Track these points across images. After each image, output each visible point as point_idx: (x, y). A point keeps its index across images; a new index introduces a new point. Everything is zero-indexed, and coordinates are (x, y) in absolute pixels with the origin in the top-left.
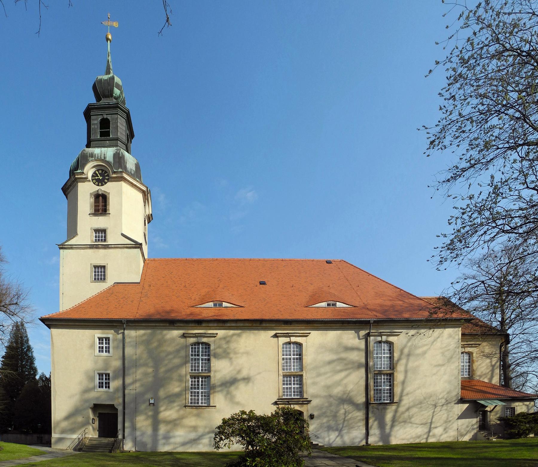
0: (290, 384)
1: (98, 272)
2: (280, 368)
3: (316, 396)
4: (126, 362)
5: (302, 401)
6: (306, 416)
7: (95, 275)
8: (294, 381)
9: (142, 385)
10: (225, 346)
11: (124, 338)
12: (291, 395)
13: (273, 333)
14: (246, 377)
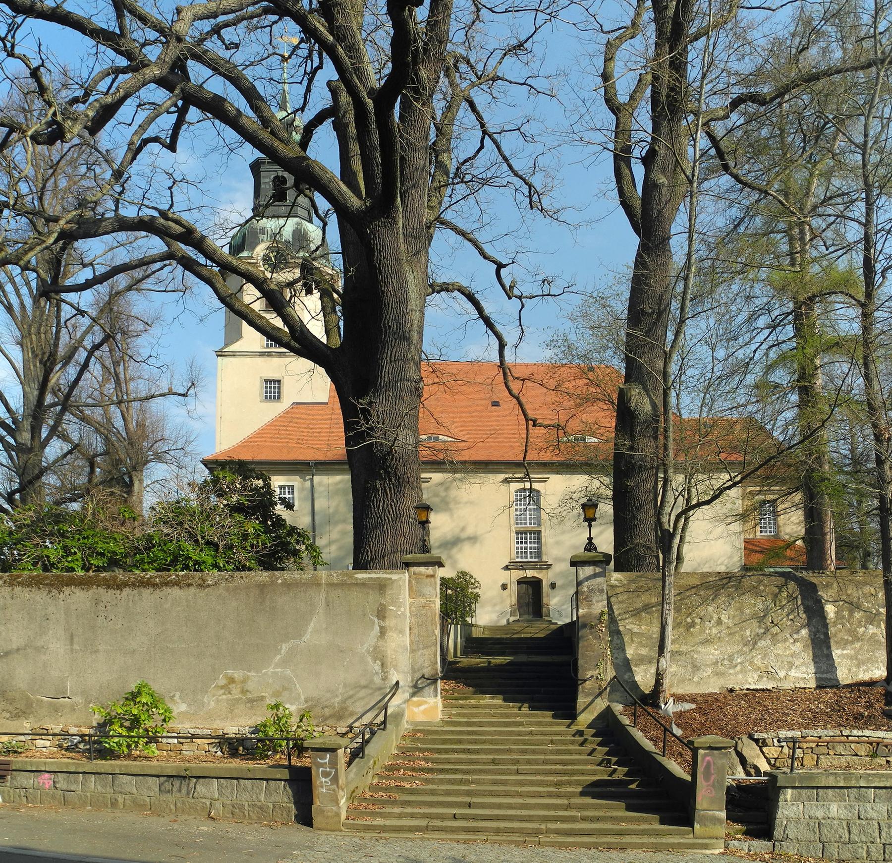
0: (526, 543)
1: (270, 388)
2: (513, 521)
3: (559, 560)
4: (317, 518)
6: (545, 585)
7: (266, 392)
8: (531, 538)
9: (340, 548)
10: (443, 494)
11: (312, 486)
12: (526, 557)
13: (502, 476)
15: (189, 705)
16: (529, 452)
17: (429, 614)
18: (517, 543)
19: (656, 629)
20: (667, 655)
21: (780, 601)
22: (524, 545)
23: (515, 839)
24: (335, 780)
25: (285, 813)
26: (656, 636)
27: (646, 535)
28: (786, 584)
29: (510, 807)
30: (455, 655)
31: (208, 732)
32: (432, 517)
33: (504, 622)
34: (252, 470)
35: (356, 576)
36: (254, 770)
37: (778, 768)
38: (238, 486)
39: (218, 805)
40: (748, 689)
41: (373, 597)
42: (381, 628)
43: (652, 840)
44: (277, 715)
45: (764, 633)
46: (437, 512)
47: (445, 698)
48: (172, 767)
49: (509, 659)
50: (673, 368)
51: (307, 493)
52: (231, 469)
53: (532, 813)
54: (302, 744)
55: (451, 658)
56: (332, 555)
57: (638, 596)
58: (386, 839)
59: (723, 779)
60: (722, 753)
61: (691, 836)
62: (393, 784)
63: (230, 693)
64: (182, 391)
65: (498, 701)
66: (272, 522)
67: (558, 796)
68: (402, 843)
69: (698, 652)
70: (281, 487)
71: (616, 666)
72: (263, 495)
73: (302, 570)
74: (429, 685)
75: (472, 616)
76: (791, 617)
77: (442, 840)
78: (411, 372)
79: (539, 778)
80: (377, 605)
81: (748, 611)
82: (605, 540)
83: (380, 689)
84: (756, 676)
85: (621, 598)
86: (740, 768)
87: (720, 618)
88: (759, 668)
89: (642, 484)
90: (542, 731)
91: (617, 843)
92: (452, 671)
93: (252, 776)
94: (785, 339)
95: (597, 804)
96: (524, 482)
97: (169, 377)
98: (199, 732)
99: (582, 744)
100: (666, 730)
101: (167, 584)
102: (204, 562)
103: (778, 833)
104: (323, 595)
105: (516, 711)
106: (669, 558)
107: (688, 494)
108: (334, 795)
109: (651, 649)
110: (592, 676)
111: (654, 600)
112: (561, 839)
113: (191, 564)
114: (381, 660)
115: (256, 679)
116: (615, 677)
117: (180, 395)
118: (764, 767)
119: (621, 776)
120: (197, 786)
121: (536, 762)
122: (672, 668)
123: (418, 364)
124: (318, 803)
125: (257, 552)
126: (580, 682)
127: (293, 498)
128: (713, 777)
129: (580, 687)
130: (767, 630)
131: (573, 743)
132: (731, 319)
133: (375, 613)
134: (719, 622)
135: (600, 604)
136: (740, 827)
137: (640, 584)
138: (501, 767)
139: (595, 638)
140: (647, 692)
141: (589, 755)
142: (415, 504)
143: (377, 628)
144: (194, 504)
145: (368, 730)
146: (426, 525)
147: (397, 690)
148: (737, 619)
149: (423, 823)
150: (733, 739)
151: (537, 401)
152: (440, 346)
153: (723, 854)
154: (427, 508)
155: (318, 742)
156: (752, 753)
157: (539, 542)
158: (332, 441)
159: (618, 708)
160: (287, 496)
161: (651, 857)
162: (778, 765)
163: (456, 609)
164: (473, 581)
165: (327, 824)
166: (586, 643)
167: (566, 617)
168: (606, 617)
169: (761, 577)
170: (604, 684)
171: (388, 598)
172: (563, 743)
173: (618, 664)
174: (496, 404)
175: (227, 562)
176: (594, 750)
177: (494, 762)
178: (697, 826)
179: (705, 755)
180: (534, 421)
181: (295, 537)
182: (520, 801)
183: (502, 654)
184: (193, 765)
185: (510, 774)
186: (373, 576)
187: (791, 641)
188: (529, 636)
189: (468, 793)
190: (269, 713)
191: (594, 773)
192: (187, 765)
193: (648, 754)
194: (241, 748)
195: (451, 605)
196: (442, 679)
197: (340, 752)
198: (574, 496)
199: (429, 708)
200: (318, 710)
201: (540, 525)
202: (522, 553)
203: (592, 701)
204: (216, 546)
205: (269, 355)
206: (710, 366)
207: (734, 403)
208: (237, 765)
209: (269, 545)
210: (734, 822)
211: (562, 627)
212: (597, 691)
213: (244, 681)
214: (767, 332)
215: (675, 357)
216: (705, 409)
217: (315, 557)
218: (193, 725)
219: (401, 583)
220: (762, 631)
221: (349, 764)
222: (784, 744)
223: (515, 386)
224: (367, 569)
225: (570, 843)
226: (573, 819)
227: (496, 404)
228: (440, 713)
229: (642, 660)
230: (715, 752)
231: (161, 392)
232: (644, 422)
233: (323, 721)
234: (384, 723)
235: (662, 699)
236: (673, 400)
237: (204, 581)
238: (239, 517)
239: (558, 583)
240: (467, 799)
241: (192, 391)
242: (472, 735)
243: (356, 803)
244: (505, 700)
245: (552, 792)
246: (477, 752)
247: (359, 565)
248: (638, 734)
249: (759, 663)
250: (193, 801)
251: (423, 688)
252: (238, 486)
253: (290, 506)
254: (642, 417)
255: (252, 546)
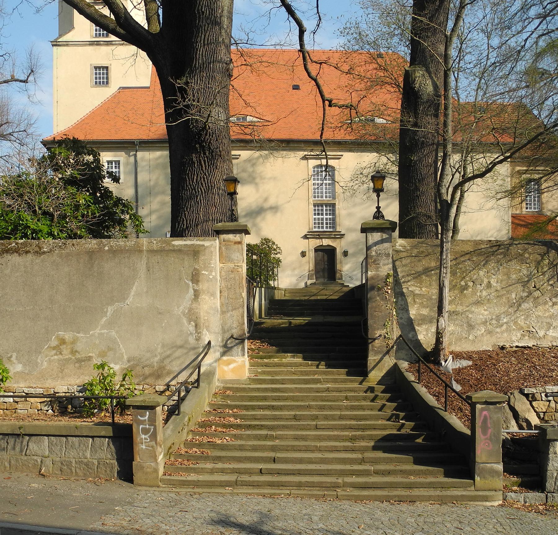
0: (322, 214)
3: (350, 230)
4: (140, 190)
5: (334, 235)
6: (338, 251)
7: (96, 78)
8: (326, 210)
9: (159, 217)
10: (250, 170)
11: (136, 161)
12: (323, 227)
13: (302, 154)
14: (273, 205)
15: (24, 365)
16: (325, 129)
17: (237, 278)
18: (315, 214)
19: (435, 291)
20: (446, 315)
21: (542, 268)
22: (320, 217)
23: (315, 492)
24: (154, 436)
25: (108, 469)
26: (435, 297)
27: (427, 206)
28: (548, 252)
29: (310, 461)
30: (260, 316)
31: (40, 391)
32: (240, 189)
33: (302, 285)
34: (83, 147)
35: (173, 243)
36: (81, 427)
37: (547, 422)
38: (72, 161)
39: (48, 462)
40: (517, 347)
41: (187, 261)
42: (195, 291)
43: (438, 493)
44: (102, 374)
45: (528, 296)
46: (243, 184)
47: (251, 357)
48: (7, 425)
49: (307, 319)
50: (453, 53)
51: (131, 167)
52: (66, 146)
53: (330, 467)
54: (125, 402)
55: (256, 319)
56: (153, 224)
57: (419, 261)
58: (200, 494)
59: (499, 432)
60: (497, 408)
61: (473, 488)
62: (205, 440)
63: (61, 353)
64: (22, 78)
65: (299, 360)
66: (101, 193)
67: (353, 450)
68: (214, 498)
69: (472, 312)
70: (109, 162)
71: (401, 326)
72: (93, 169)
73: (126, 237)
74: (237, 344)
75: (274, 280)
76: (551, 282)
77: (250, 494)
78: (222, 54)
79: (336, 433)
80: (192, 270)
81: (514, 276)
82: (392, 211)
83: (194, 349)
84: (519, 335)
85: (404, 262)
86: (513, 422)
87: (489, 282)
88: (522, 328)
89: (424, 159)
90: (338, 388)
91: (407, 496)
92: (257, 332)
93: (79, 434)
94: (554, 28)
95: (388, 458)
96: (321, 159)
97: (11, 65)
98: (32, 391)
99: (373, 400)
100: (447, 386)
101: (7, 251)
102: (40, 231)
103: (550, 485)
104: (144, 261)
105: (314, 368)
106: (446, 227)
107: (464, 170)
108: (154, 450)
109: (431, 310)
110: (380, 336)
111: (433, 264)
112: (356, 492)
113: (29, 232)
114: (195, 321)
115: (84, 340)
116: (401, 336)
117: (21, 81)
118: (535, 421)
119: (408, 431)
120: (30, 444)
121: (333, 418)
122: (450, 328)
123: (228, 47)
124: (139, 460)
125: (87, 222)
126: (370, 341)
127: (119, 172)
128: (490, 431)
129: (370, 346)
130: (530, 293)
131: (365, 399)
132: (505, 10)
133: (190, 278)
134: (489, 285)
135: (386, 267)
136: (515, 479)
137: (421, 249)
138: (301, 423)
139: (382, 299)
140: (429, 350)
141: (380, 410)
142: (225, 177)
143: (191, 292)
144: (33, 177)
145: (183, 388)
146: (234, 196)
147: (209, 349)
148: (504, 283)
149: (232, 478)
150: (506, 394)
151: (333, 83)
152: (247, 31)
153: (502, 506)
154: (235, 181)
155: (138, 400)
156: (524, 408)
157: (334, 214)
158: (153, 121)
159: (404, 365)
160: (114, 170)
161: (438, 509)
162: (546, 418)
163: (260, 272)
164: (275, 247)
165: (146, 479)
166: (374, 304)
167: (357, 280)
168: (391, 280)
169: (526, 246)
170: (391, 343)
171: (201, 262)
172: (356, 399)
173: (403, 324)
174: (296, 87)
175: (61, 231)
176: (384, 405)
177: (295, 418)
178: (477, 479)
179: (482, 410)
180: (330, 101)
181: (121, 207)
182: (319, 455)
183: (301, 315)
184: (26, 423)
185: (309, 429)
186: (188, 242)
187: (550, 304)
188: (325, 297)
189: (273, 449)
190: (96, 372)
191: (384, 428)
192: (21, 423)
193: (432, 409)
194: (70, 406)
195: (256, 270)
196: (249, 338)
197: (159, 409)
198: (365, 172)
199: (237, 367)
200: (139, 369)
201: (334, 198)
202: (319, 224)
203: (381, 359)
204: (52, 215)
205: (98, 43)
206: (485, 54)
207: (506, 89)
208: (66, 423)
209: (97, 215)
210: (510, 474)
211: (353, 290)
212: (385, 350)
213: (74, 342)
214: (537, 22)
215: (455, 42)
216: (481, 93)
217: (137, 226)
218: (27, 384)
219: (212, 249)
220: (526, 294)
221: (166, 421)
222: (551, 398)
223: (313, 69)
224: (182, 236)
225: (364, 496)
226: (366, 473)
227: (296, 87)
228: (247, 371)
229: (424, 320)
230: (491, 406)
231: (5, 79)
232: (427, 102)
233: (143, 380)
234: (198, 381)
235: (442, 357)
236: (452, 84)
237: (40, 248)
238: (72, 190)
239: (350, 251)
240: (272, 454)
241: (31, 78)
242: (276, 392)
243: (172, 459)
244: (305, 358)
245: (348, 447)
246: (280, 408)
247: (176, 233)
248: (422, 390)
249: (522, 324)
250: (26, 458)
251: (232, 347)
252: (72, 161)
253: (116, 179)
254: (425, 98)
255: (83, 216)
